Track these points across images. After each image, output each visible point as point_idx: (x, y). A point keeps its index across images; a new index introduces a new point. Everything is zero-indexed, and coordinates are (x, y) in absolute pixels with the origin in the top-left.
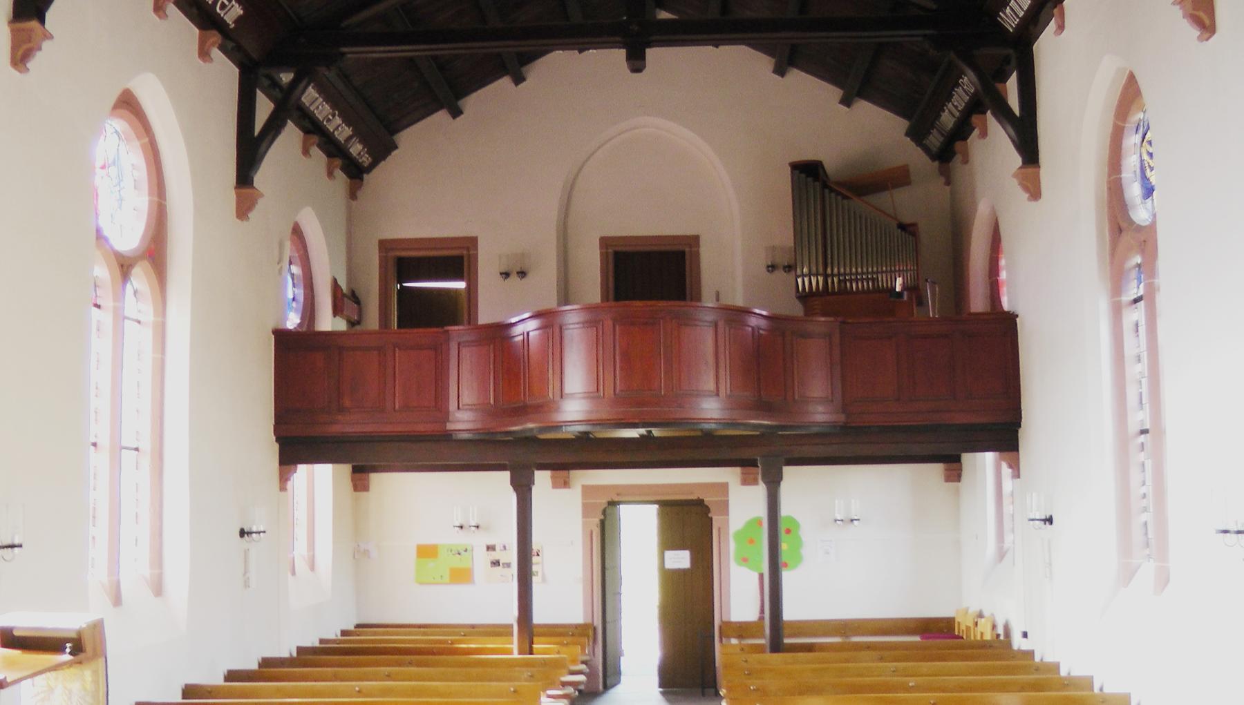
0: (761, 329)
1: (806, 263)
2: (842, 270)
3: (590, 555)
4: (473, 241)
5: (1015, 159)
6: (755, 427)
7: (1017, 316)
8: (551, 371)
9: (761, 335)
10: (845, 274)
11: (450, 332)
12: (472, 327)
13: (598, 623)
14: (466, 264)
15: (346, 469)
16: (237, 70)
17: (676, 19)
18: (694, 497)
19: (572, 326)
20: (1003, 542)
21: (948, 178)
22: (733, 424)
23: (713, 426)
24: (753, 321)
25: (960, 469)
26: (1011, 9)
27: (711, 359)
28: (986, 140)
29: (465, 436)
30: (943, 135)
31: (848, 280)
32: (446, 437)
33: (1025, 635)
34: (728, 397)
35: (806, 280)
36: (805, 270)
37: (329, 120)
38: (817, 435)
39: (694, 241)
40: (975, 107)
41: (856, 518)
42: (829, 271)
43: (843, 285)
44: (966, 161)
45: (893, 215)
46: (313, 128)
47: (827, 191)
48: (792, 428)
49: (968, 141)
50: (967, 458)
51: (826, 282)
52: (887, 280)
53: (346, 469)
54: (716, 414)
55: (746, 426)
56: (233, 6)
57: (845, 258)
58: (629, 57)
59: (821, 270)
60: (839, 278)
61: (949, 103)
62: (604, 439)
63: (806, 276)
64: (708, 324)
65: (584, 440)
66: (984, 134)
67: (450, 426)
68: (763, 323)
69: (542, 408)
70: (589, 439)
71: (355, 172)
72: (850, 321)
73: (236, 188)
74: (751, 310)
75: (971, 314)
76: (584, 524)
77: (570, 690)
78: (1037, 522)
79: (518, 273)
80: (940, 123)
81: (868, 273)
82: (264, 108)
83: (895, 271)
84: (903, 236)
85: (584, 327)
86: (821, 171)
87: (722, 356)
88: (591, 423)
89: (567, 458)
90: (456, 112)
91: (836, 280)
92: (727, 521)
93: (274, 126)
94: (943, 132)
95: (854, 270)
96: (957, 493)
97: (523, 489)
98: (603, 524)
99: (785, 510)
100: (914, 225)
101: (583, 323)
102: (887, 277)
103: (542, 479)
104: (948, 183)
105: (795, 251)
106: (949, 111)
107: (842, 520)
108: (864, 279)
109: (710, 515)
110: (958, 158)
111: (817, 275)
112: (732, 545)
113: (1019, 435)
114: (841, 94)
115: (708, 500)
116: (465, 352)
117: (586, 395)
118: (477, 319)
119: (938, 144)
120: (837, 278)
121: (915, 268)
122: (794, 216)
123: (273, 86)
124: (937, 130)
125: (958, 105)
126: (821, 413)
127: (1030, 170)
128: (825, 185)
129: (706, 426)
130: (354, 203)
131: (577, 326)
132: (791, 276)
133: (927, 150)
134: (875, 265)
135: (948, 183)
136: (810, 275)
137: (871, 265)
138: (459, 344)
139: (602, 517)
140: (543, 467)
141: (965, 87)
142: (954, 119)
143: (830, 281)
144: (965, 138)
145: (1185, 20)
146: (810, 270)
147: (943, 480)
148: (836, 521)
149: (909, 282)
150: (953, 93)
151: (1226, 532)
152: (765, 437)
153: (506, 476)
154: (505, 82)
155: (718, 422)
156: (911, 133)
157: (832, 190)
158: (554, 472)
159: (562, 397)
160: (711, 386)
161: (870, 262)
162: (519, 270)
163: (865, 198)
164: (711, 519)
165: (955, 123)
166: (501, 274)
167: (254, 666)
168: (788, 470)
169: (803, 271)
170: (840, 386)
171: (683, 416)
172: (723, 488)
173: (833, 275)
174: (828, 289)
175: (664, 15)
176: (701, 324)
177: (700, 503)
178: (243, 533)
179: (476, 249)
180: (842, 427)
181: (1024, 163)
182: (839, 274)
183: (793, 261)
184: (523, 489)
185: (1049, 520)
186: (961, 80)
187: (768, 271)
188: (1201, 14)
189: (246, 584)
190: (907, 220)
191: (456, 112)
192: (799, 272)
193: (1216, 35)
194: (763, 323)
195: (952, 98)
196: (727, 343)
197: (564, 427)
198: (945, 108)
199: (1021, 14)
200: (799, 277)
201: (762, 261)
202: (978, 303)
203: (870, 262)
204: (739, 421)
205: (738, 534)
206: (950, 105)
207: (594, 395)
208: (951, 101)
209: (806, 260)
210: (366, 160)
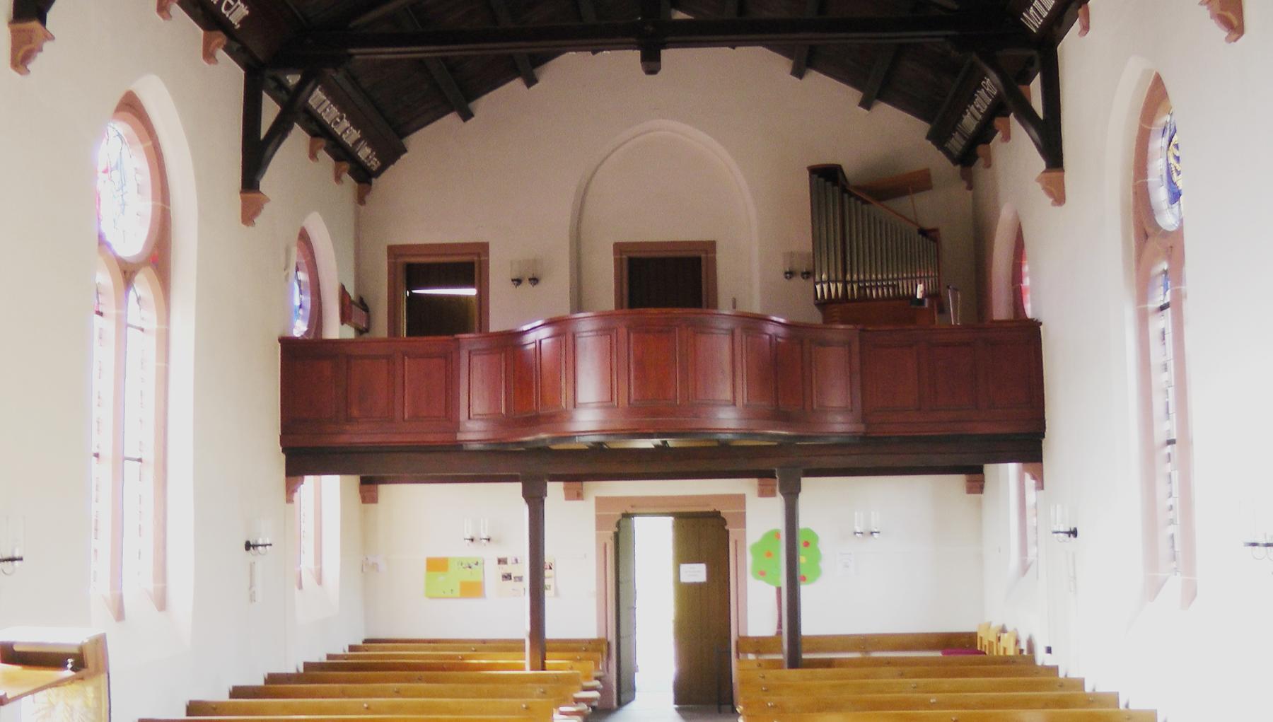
0: (779, 337)
1: (825, 270)
2: (862, 277)
3: (603, 569)
4: (484, 247)
5: (1039, 163)
6: (773, 437)
7: (1041, 324)
8: (563, 380)
9: (779, 343)
10: (865, 281)
11: (461, 340)
12: (483, 335)
13: (612, 638)
14: (476, 270)
15: (354, 480)
16: (242, 72)
18: (710, 509)
19: (585, 334)
20: (1027, 555)
21: (970, 183)
22: (750, 435)
23: (730, 436)
24: (771, 329)
25: (983, 481)
26: (1035, 9)
27: (727, 367)
28: (1009, 143)
29: (476, 446)
30: (965, 138)
31: (868, 287)
32: (456, 448)
33: (1049, 650)
34: (745, 406)
35: (825, 286)
36: (824, 277)
37: (336, 123)
38: (836, 445)
39: (711, 246)
40: (998, 109)
41: (876, 530)
42: (848, 277)
43: (862, 291)
44: (988, 164)
45: (914, 220)
46: (320, 131)
47: (846, 196)
48: (810, 438)
49: (991, 144)
50: (989, 469)
51: (845, 289)
52: (908, 287)
53: (354, 480)
54: (733, 424)
55: (763, 436)
56: (238, 6)
57: (864, 264)
58: (644, 59)
59: (840, 277)
60: (859, 285)
61: (971, 105)
62: (618, 449)
63: (824, 282)
64: (724, 332)
65: (597, 451)
66: (1007, 137)
67: (460, 437)
68: (781, 331)
69: (555, 417)
70: (603, 450)
71: (364, 177)
72: (870, 329)
73: (241, 192)
74: (768, 318)
75: (993, 322)
76: (598, 537)
78: (1061, 535)
79: (530, 279)
80: (962, 126)
81: (888, 279)
82: (270, 110)
83: (916, 277)
84: (924, 242)
85: (597, 335)
86: (840, 175)
87: (738, 365)
88: (605, 433)
89: (581, 469)
90: (467, 115)
91: (855, 287)
92: (744, 534)
93: (280, 129)
94: (965, 135)
95: (874, 276)
96: (980, 505)
97: (535, 501)
98: (617, 536)
99: (804, 522)
100: (936, 230)
101: (597, 331)
102: (907, 284)
103: (555, 490)
104: (970, 187)
105: (814, 257)
106: (971, 113)
107: (862, 533)
108: (884, 286)
109: (726, 528)
110: (980, 162)
111: (836, 281)
112: (749, 558)
113: (1043, 445)
114: (861, 97)
115: (724, 512)
116: (476, 360)
117: (600, 405)
118: (488, 327)
119: (960, 148)
120: (857, 284)
121: (937, 274)
122: (813, 221)
123: (279, 88)
124: (959, 133)
125: (981, 108)
126: (840, 423)
127: (1054, 174)
128: (844, 190)
129: (723, 437)
130: (362, 208)
131: (590, 334)
132: (810, 283)
133: (948, 153)
134: (895, 272)
135: (970, 187)
136: (828, 281)
137: (891, 272)
138: (470, 352)
139: (616, 530)
140: (555, 478)
141: (988, 89)
142: (977, 122)
143: (849, 288)
144: (988, 142)
145: (1213, 21)
146: (829, 277)
147: (965, 492)
148: (855, 533)
149: (930, 289)
150: (976, 95)
151: (1254, 544)
152: (783, 447)
153: (517, 487)
154: (517, 84)
155: (735, 432)
156: (932, 136)
157: (851, 195)
158: (566, 483)
159: (575, 407)
160: (727, 395)
161: (890, 269)
162: (531, 276)
163: (885, 203)
164: (728, 532)
165: (977, 126)
166: (513, 280)
167: (260, 682)
168: (806, 482)
169: (821, 278)
170: (860, 395)
171: (699, 426)
172: (740, 500)
173: (852, 282)
174: (847, 296)
175: (679, 15)
176: (717, 331)
177: (716, 515)
178: (248, 546)
179: (487, 255)
180: (861, 437)
181: (1048, 167)
182: (859, 281)
183: (811, 268)
184: (535, 501)
185: (1074, 533)
186: (983, 82)
187: (786, 278)
188: (1229, 15)
189: (252, 599)
190: (928, 225)
191: (467, 115)
192: (817, 278)
193: (1244, 36)
194: (781, 331)
195: (974, 100)
196: (744, 351)
197: (577, 438)
198: (967, 110)
199: (1045, 14)
200: (817, 283)
201: (779, 268)
202: (1001, 310)
203: (890, 269)
204: (757, 431)
205: (755, 546)
206: (972, 108)
207: (608, 405)
208: (973, 104)
209: (825, 266)
210: (374, 164)
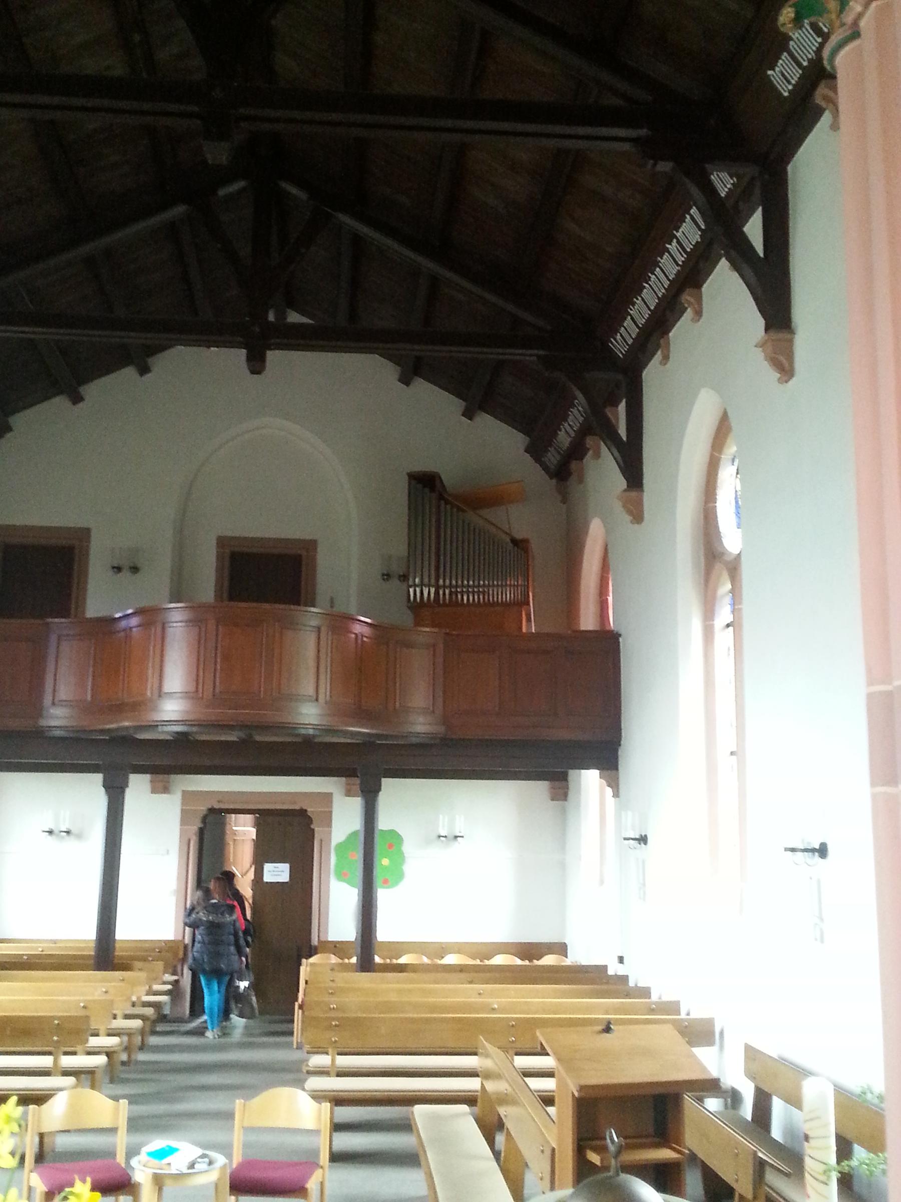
1: (418, 574)
2: (454, 582)
4: (84, 534)
5: (621, 482)
6: (353, 734)
7: (620, 635)
9: (365, 641)
17: (312, 324)
19: (175, 625)
23: (311, 732)
24: (358, 628)
26: (621, 335)
27: (312, 663)
29: (58, 733)
30: (559, 453)
32: (39, 735)
33: (621, 960)
35: (418, 590)
39: (311, 545)
40: (585, 431)
42: (441, 582)
43: (454, 597)
44: (581, 480)
45: (508, 532)
47: (442, 502)
51: (437, 593)
52: (498, 594)
54: (314, 721)
55: (346, 733)
58: (250, 359)
59: (433, 581)
63: (418, 586)
64: (311, 629)
65: (182, 741)
66: (597, 455)
67: (43, 723)
68: (366, 630)
69: (137, 706)
70: (188, 741)
76: (182, 833)
77: (150, 1011)
78: (631, 841)
79: (131, 568)
81: (457, 586)
83: (506, 585)
85: (187, 626)
88: (187, 723)
90: (77, 399)
91: (447, 591)
92: (330, 833)
95: (466, 582)
96: (564, 812)
99: (383, 823)
100: (525, 541)
101: (190, 621)
107: (446, 837)
108: (476, 592)
109: (312, 827)
110: (574, 478)
111: (429, 586)
113: (620, 753)
116: (65, 647)
117: (184, 694)
118: (84, 612)
124: (555, 448)
125: (574, 425)
127: (634, 494)
128: (441, 497)
129: (303, 732)
131: (180, 624)
132: (404, 586)
133: (546, 468)
134: (471, 578)
136: (422, 585)
137: (442, 576)
142: (569, 440)
143: (441, 592)
144: (581, 458)
145: (766, 362)
148: (439, 837)
151: (793, 850)
152: (367, 746)
153: (98, 778)
154: (129, 373)
155: (315, 727)
157: (447, 502)
160: (310, 690)
161: (454, 573)
162: (132, 565)
163: (478, 512)
164: (313, 830)
165: (571, 442)
166: (114, 568)
168: (385, 782)
169: (415, 581)
172: (327, 798)
173: (444, 587)
175: (294, 317)
176: (304, 628)
177: (302, 813)
182: (451, 586)
185: (643, 840)
187: (384, 579)
188: (782, 358)
190: (519, 536)
191: (77, 399)
192: (411, 583)
193: (794, 379)
194: (366, 630)
197: (160, 727)
198: (562, 427)
199: (630, 342)
200: (411, 586)
202: (588, 622)
203: (454, 573)
205: (339, 846)
207: (194, 695)
208: (567, 421)
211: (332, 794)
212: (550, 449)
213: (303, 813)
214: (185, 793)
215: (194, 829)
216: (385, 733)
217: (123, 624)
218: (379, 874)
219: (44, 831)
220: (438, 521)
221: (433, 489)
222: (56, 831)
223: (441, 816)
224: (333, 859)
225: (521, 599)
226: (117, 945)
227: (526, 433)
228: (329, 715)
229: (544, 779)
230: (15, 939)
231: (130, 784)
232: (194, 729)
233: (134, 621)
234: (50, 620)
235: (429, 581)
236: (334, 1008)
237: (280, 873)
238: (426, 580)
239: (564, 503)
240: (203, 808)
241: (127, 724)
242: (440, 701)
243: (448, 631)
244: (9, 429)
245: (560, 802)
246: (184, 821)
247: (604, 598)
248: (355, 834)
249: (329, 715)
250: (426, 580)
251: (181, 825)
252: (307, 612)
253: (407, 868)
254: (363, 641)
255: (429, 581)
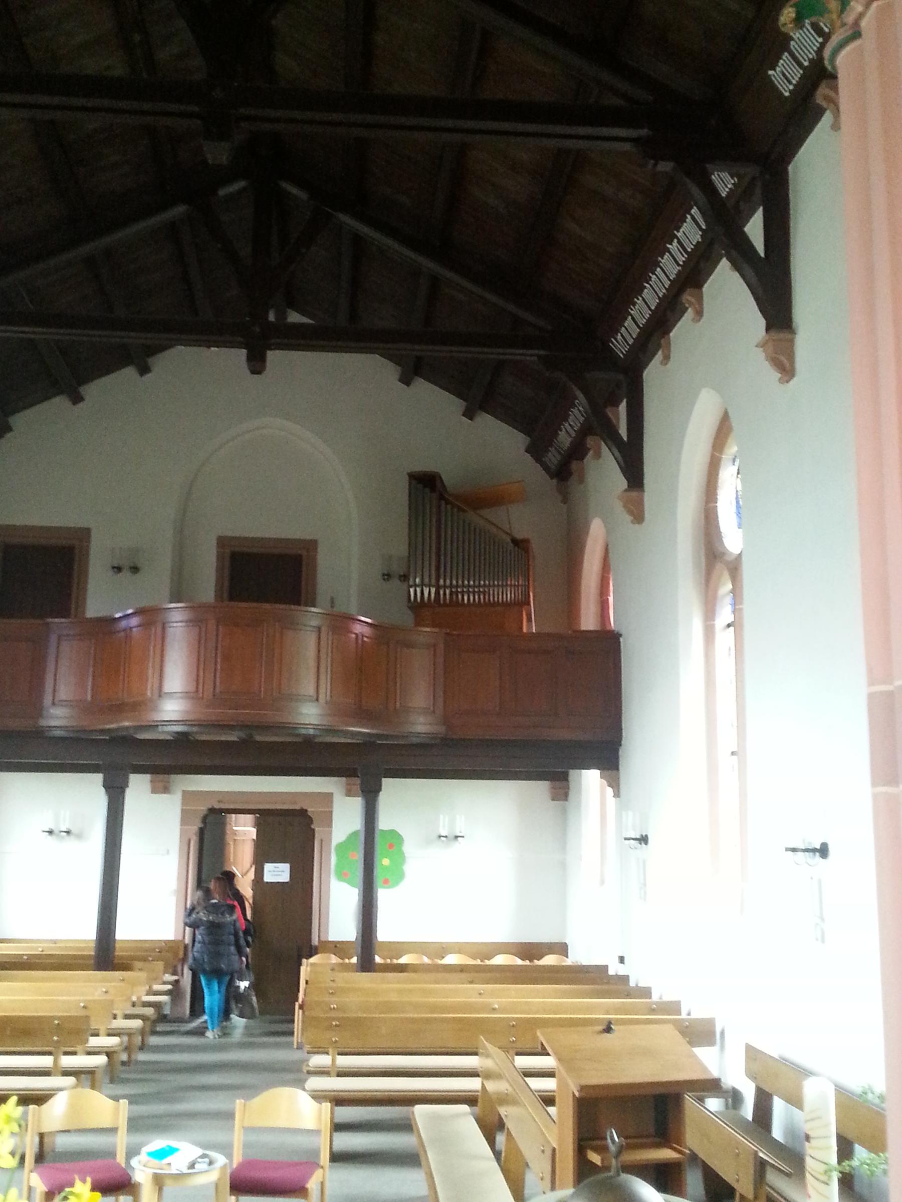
1: (419, 574)
2: (454, 582)
4: (84, 534)
5: (621, 482)
6: (353, 734)
7: (621, 635)
9: (365, 641)
19: (175, 625)
23: (311, 732)
24: (358, 628)
26: (622, 335)
27: (312, 663)
29: (58, 733)
30: (560, 453)
32: (39, 735)
33: (622, 960)
35: (418, 590)
39: (311, 545)
40: (586, 431)
42: (442, 582)
43: (454, 597)
44: (582, 480)
45: (509, 532)
47: (443, 502)
51: (437, 593)
52: (498, 594)
54: (315, 721)
55: (346, 733)
58: (250, 359)
59: (433, 581)
63: (418, 586)
64: (311, 629)
65: (182, 741)
66: (598, 455)
67: (43, 723)
68: (366, 630)
69: (138, 706)
70: (189, 741)
76: (182, 833)
78: (632, 841)
79: (131, 568)
81: (457, 586)
83: (507, 585)
85: (188, 626)
88: (187, 723)
90: (77, 399)
91: (448, 591)
92: (330, 833)
95: (466, 582)
96: (564, 812)
99: (384, 823)
100: (526, 541)
101: (190, 621)
107: (446, 837)
108: (476, 592)
109: (313, 827)
110: (574, 478)
111: (430, 586)
113: (620, 753)
116: (65, 647)
117: (184, 694)
118: (84, 612)
124: (556, 448)
125: (575, 425)
127: (634, 494)
128: (441, 497)
129: (303, 732)
131: (180, 624)
132: (405, 586)
133: (546, 468)
134: (472, 578)
136: (422, 585)
137: (442, 576)
142: (570, 440)
143: (442, 592)
144: (582, 458)
145: (767, 362)
148: (440, 837)
151: (794, 850)
152: (367, 746)
153: (98, 778)
154: (129, 373)
155: (315, 727)
157: (447, 502)
160: (311, 690)
161: (454, 573)
162: (132, 565)
163: (478, 512)
164: (313, 830)
165: (572, 442)
166: (114, 568)
168: (386, 782)
169: (415, 581)
172: (327, 798)
173: (445, 587)
175: (294, 317)
176: (304, 628)
177: (303, 813)
182: (451, 586)
185: (644, 840)
187: (384, 579)
188: (782, 358)
190: (519, 536)
191: (77, 399)
192: (411, 583)
193: (795, 379)
194: (366, 630)
197: (160, 727)
198: (562, 427)
199: (631, 342)
200: (411, 586)
202: (588, 622)
203: (454, 573)
205: (339, 846)
207: (194, 695)
208: (567, 421)
211: (332, 794)
212: (550, 449)
213: (303, 813)
214: (185, 793)
215: (194, 829)
216: (385, 733)
217: (123, 624)
218: (379, 874)
219: (44, 831)
220: (439, 521)
221: (433, 489)
222: (56, 831)
223: (441, 816)
224: (334, 859)
225: (522, 599)
226: (117, 945)
227: (527, 433)
228: (329, 715)
229: (545, 779)
230: (15, 939)
231: (130, 784)
232: (195, 729)
233: (134, 621)
234: (50, 620)
235: (430, 581)
236: (334, 1008)
237: (280, 873)
238: (426, 580)
239: (565, 503)
240: (203, 808)
241: (127, 724)
242: (440, 701)
243: (448, 631)
244: (9, 429)
245: (561, 802)
246: (184, 821)
247: (604, 598)
248: (355, 834)
249: (329, 715)
250: (426, 580)
251: (181, 825)
252: (307, 612)
253: (408, 868)
254: (363, 641)
255: (430, 581)
